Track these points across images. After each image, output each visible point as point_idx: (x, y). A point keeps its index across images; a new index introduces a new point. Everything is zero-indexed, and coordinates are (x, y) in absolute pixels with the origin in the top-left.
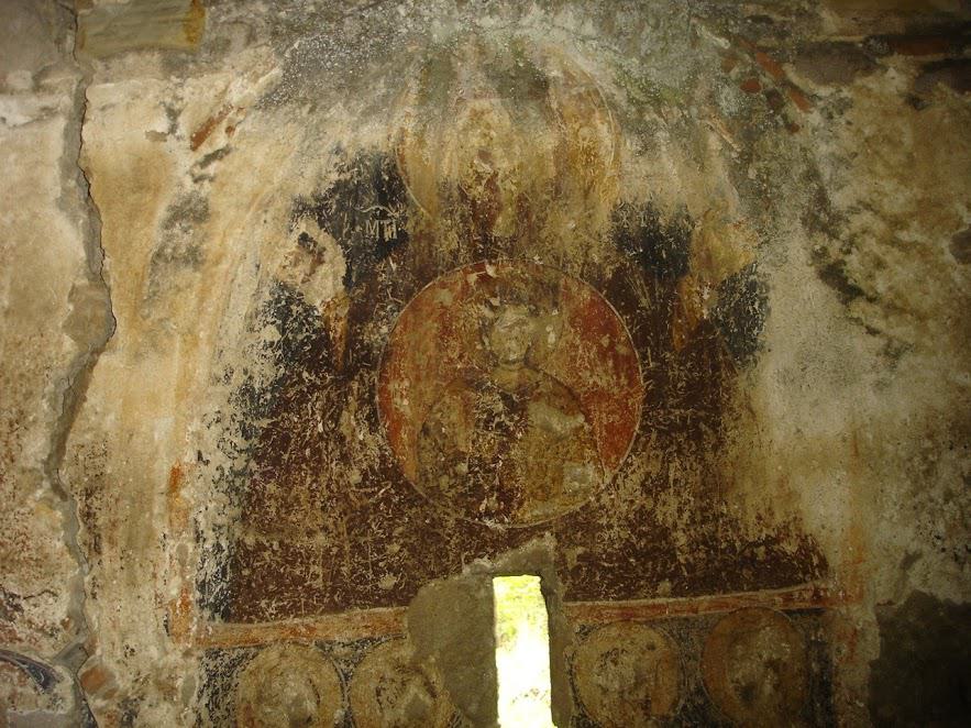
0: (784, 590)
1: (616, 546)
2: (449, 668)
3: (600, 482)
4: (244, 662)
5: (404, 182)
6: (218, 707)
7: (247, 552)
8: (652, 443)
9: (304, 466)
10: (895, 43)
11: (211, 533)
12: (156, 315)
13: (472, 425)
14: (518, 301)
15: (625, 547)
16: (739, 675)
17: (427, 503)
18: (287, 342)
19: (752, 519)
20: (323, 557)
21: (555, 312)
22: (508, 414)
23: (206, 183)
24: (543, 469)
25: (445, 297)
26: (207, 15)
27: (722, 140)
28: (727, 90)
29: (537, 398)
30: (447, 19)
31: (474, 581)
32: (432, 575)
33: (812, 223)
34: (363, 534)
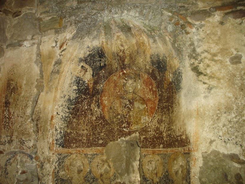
0: (184, 148)
1: (152, 136)
2: (114, 162)
4: (67, 157)
5: (105, 53)
6: (60, 165)
7: (68, 134)
10: (218, 8)
12: (51, 84)
14: (131, 78)
15: (154, 136)
16: (175, 168)
17: (110, 124)
18: (79, 89)
19: (177, 130)
21: (140, 81)
22: (130, 104)
23: (62, 56)
24: (137, 117)
25: (115, 78)
26: (63, 21)
27: (169, 38)
28: (170, 25)
29: (136, 101)
30: (107, 16)
31: (121, 142)
32: (111, 141)
33: (191, 57)
34: (95, 131)
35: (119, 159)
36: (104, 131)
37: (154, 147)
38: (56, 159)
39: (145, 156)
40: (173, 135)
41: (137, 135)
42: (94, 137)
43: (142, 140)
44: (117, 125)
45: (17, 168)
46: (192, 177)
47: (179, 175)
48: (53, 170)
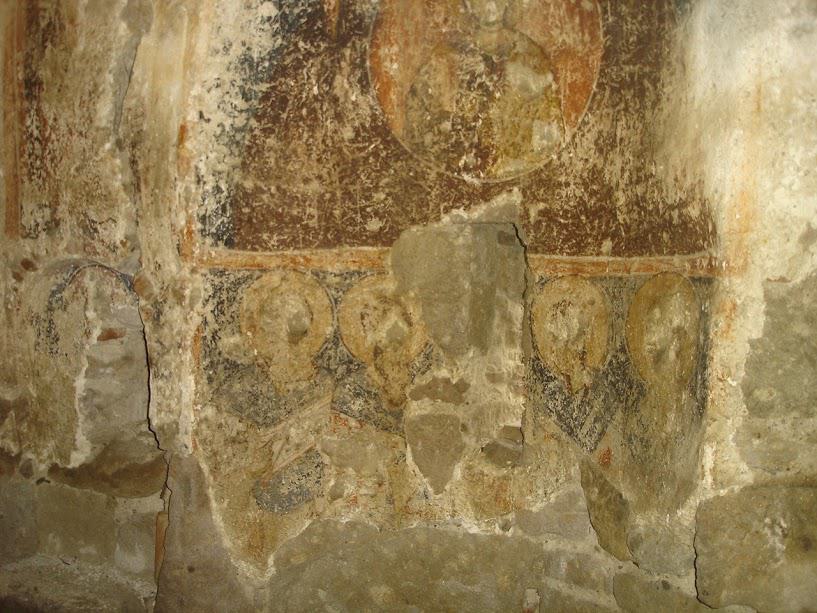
0: (691, 256)
1: (572, 203)
2: (427, 302)
3: (562, 140)
6: (223, 313)
8: (605, 101)
9: (301, 123)
11: (211, 177)
13: (456, 86)
16: (654, 339)
17: (411, 157)
18: (284, 16)
19: (670, 180)
20: (318, 201)
29: (514, 60)
32: (413, 222)
34: (353, 183)
35: (443, 293)
36: (387, 184)
37: (580, 249)
38: (206, 290)
39: (543, 282)
40: (653, 203)
41: (515, 198)
42: (348, 208)
43: (532, 220)
44: (438, 158)
45: (87, 318)
46: (712, 381)
47: (669, 367)
48: (193, 328)
